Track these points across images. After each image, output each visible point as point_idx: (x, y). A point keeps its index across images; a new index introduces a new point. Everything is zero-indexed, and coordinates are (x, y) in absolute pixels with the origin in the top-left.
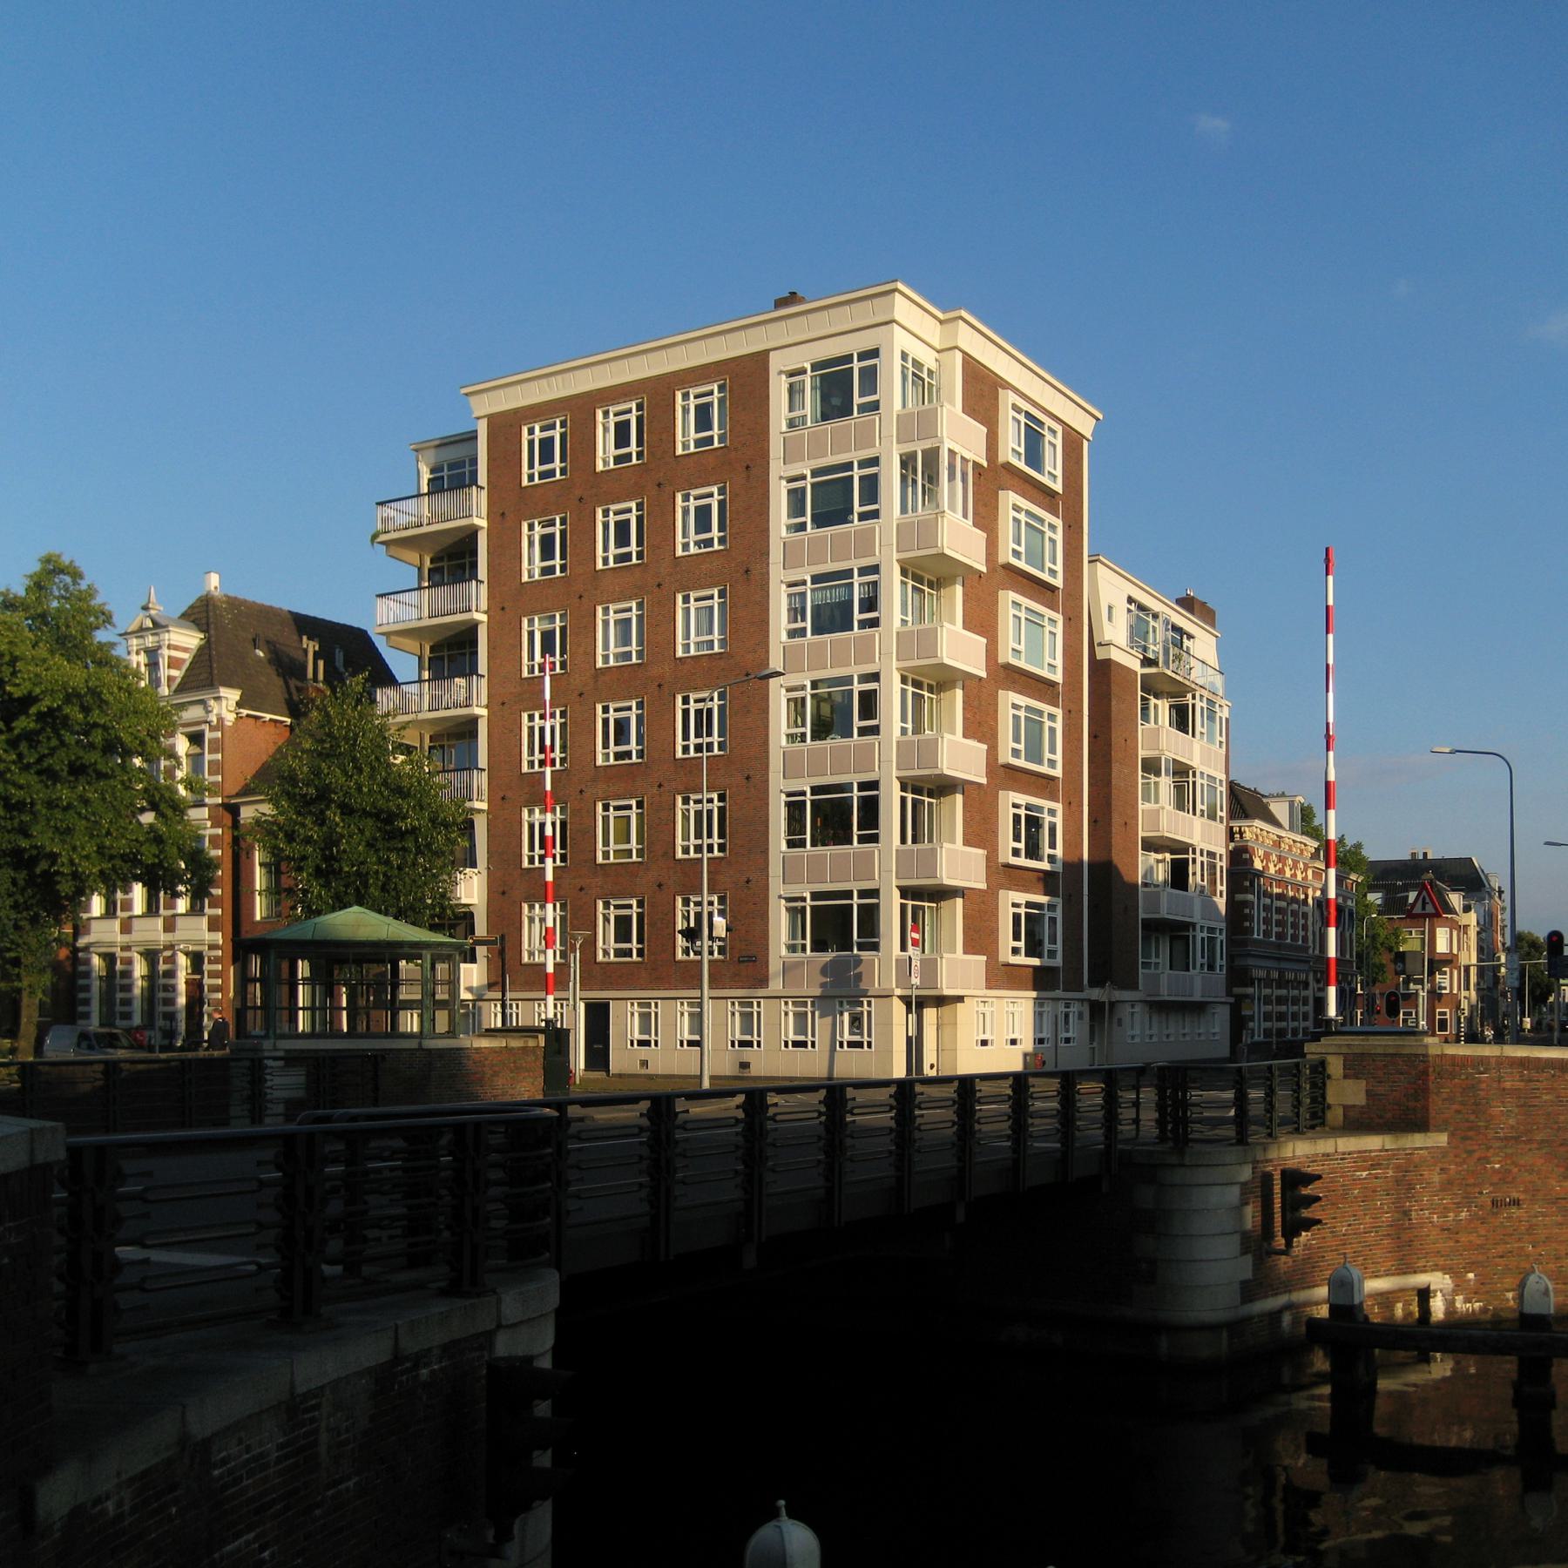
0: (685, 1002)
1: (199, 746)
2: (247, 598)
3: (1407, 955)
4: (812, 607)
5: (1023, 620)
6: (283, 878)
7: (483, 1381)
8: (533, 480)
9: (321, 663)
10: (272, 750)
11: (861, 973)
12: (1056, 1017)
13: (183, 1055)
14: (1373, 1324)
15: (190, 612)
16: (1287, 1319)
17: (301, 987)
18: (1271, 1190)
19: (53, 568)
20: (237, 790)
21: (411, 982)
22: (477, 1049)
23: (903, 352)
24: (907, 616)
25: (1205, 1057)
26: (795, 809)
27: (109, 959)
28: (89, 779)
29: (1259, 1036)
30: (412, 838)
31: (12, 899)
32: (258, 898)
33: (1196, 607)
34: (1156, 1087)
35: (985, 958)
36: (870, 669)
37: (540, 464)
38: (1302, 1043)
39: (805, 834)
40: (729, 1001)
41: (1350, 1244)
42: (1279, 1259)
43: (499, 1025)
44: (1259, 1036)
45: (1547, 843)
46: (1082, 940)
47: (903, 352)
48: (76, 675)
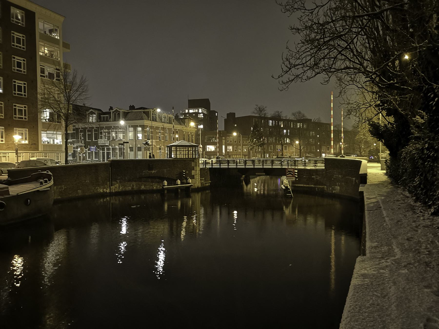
0: (44, 153)
1: (58, 45)
2: (346, 302)
4: (337, 270)
7: (77, 195)
8: (14, 82)
12: (44, 66)
13: (78, 156)
14: (195, 123)
16: (378, 140)
18: (225, 149)
19: (261, 110)
20: (129, 113)
24: (24, 86)
27: (398, 238)
28: (395, 224)
29: (293, 179)
32: (299, 168)
33: (2, 135)
37: (22, 92)
39: (105, 117)
40: (29, 153)
41: (88, 98)
42: (285, 183)
43: (191, 157)
44: (293, 179)
46: (27, 89)
48: (83, 121)
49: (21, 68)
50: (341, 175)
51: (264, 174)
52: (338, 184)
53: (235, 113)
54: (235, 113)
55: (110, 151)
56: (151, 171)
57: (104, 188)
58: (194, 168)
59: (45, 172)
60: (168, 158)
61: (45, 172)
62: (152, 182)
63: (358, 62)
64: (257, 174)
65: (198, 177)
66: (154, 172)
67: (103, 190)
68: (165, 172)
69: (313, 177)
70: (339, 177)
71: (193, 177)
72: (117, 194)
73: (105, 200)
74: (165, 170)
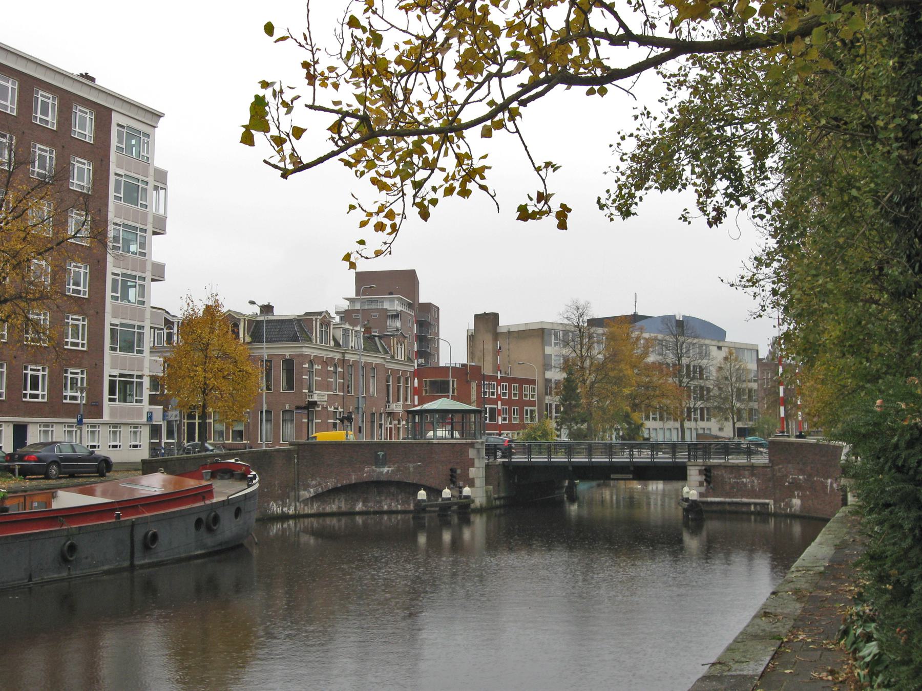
3: (545, 331)
5: (121, 231)
6: (170, 413)
9: (416, 397)
10: (718, 565)
11: (468, 89)
15: (593, 32)
17: (613, 460)
21: (390, 520)
22: (67, 221)
23: (361, 226)
25: (635, 62)
26: (112, 384)
30: (246, 341)
31: (846, 353)
34: (638, 434)
35: (162, 407)
36: (140, 373)
38: (709, 188)
45: (299, 97)
47: (361, 226)
49: (7, 101)
50: (803, 474)
51: (631, 476)
52: (798, 495)
53: (476, 316)
54: (476, 316)
55: (17, 467)
56: (381, 470)
57: (284, 505)
58: (474, 463)
59: (233, 461)
60: (408, 438)
61: (233, 461)
62: (379, 493)
63: (660, 51)
64: (612, 476)
65: (480, 482)
66: (388, 471)
67: (282, 509)
68: (411, 469)
69: (744, 480)
70: (800, 479)
71: (471, 484)
72: (339, 514)
73: (285, 525)
74: (411, 466)
